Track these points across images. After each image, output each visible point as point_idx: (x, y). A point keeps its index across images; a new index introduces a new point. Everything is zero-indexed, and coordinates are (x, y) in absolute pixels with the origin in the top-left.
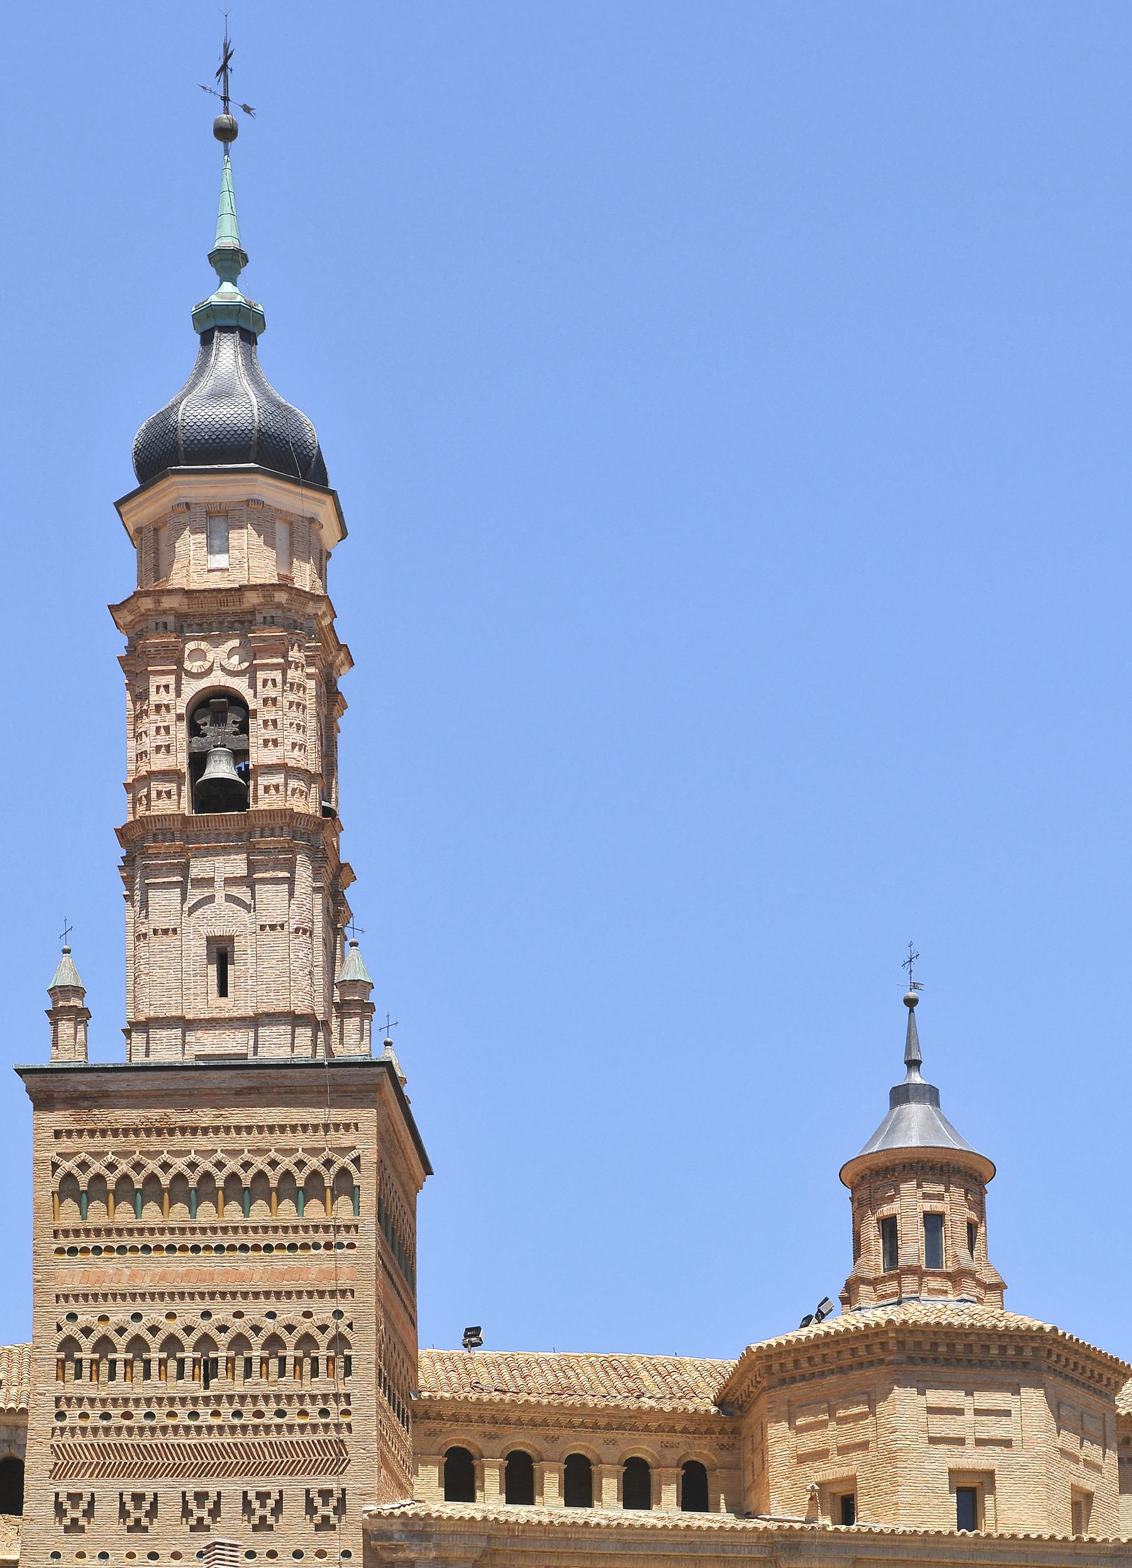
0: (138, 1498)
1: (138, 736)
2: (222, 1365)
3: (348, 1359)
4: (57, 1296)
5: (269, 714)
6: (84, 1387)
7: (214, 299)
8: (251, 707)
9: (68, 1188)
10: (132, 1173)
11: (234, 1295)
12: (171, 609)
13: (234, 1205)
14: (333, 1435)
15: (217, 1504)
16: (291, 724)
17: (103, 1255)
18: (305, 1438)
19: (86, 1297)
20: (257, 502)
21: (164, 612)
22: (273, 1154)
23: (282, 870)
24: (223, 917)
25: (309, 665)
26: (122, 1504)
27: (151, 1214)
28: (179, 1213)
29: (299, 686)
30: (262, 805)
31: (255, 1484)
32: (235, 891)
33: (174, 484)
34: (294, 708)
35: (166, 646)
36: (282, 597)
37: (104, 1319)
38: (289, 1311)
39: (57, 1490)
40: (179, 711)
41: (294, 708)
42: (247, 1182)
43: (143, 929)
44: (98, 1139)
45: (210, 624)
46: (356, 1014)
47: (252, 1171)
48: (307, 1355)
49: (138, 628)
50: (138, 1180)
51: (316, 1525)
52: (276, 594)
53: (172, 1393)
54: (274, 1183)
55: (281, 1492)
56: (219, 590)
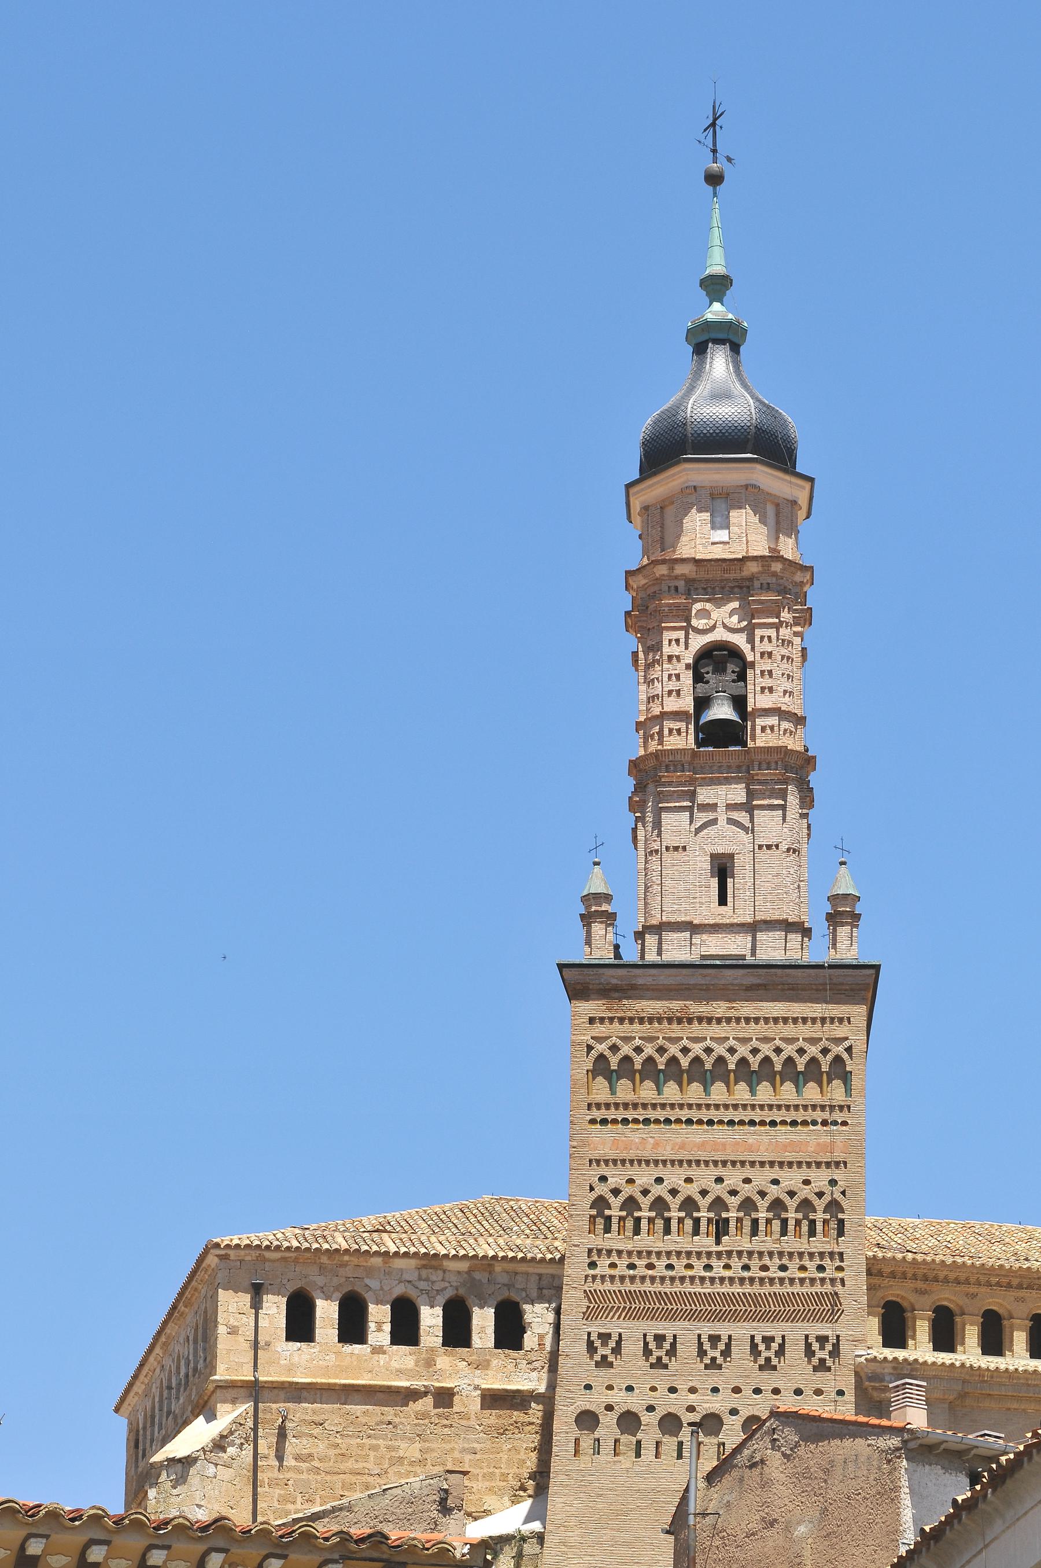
0: (660, 1339)
1: (649, 682)
2: (732, 1224)
3: (841, 1223)
4: (591, 1161)
5: (765, 665)
6: (613, 1241)
7: (709, 316)
8: (750, 658)
9: (601, 1067)
10: (656, 1056)
11: (743, 1163)
12: (682, 575)
13: (742, 1086)
14: (828, 1288)
15: (728, 1345)
16: (783, 674)
17: (630, 1126)
18: (804, 1290)
19: (615, 1162)
20: (754, 486)
21: (676, 577)
22: (778, 1042)
23: (777, 798)
24: (725, 838)
25: (796, 624)
26: (646, 1344)
27: (671, 1091)
28: (695, 1091)
29: (789, 642)
30: (760, 743)
31: (762, 1329)
32: (735, 815)
33: (684, 470)
34: (785, 660)
35: (677, 606)
36: (777, 567)
37: (631, 1181)
38: (791, 1179)
39: (589, 1330)
40: (687, 662)
41: (785, 660)
42: (755, 1067)
43: (656, 846)
44: (626, 1025)
45: (714, 588)
46: (847, 924)
47: (760, 1056)
48: (806, 1217)
49: (650, 591)
50: (661, 1062)
51: (814, 1367)
52: (773, 564)
53: (689, 1247)
54: (778, 1067)
55: (783, 1337)
56: (724, 560)
